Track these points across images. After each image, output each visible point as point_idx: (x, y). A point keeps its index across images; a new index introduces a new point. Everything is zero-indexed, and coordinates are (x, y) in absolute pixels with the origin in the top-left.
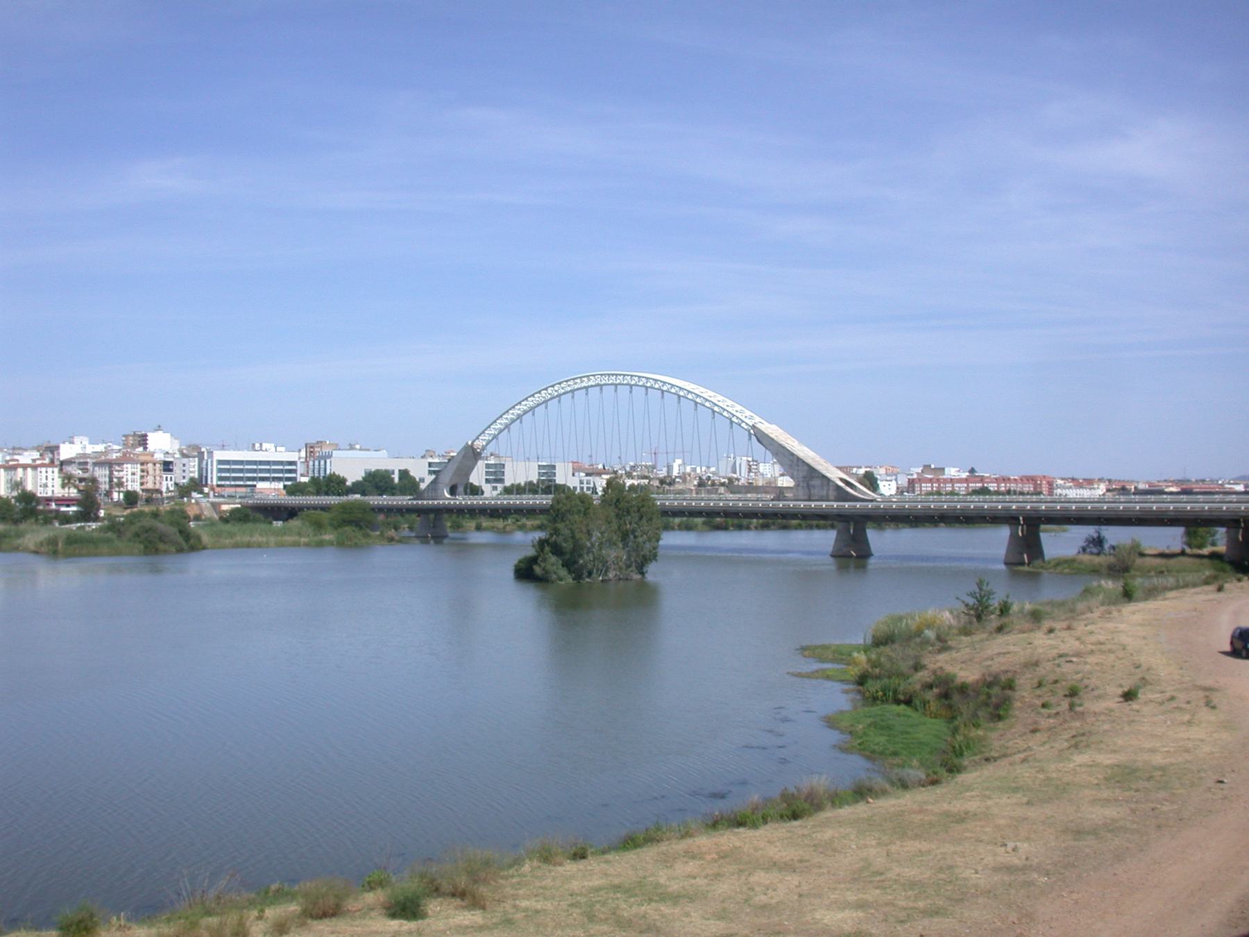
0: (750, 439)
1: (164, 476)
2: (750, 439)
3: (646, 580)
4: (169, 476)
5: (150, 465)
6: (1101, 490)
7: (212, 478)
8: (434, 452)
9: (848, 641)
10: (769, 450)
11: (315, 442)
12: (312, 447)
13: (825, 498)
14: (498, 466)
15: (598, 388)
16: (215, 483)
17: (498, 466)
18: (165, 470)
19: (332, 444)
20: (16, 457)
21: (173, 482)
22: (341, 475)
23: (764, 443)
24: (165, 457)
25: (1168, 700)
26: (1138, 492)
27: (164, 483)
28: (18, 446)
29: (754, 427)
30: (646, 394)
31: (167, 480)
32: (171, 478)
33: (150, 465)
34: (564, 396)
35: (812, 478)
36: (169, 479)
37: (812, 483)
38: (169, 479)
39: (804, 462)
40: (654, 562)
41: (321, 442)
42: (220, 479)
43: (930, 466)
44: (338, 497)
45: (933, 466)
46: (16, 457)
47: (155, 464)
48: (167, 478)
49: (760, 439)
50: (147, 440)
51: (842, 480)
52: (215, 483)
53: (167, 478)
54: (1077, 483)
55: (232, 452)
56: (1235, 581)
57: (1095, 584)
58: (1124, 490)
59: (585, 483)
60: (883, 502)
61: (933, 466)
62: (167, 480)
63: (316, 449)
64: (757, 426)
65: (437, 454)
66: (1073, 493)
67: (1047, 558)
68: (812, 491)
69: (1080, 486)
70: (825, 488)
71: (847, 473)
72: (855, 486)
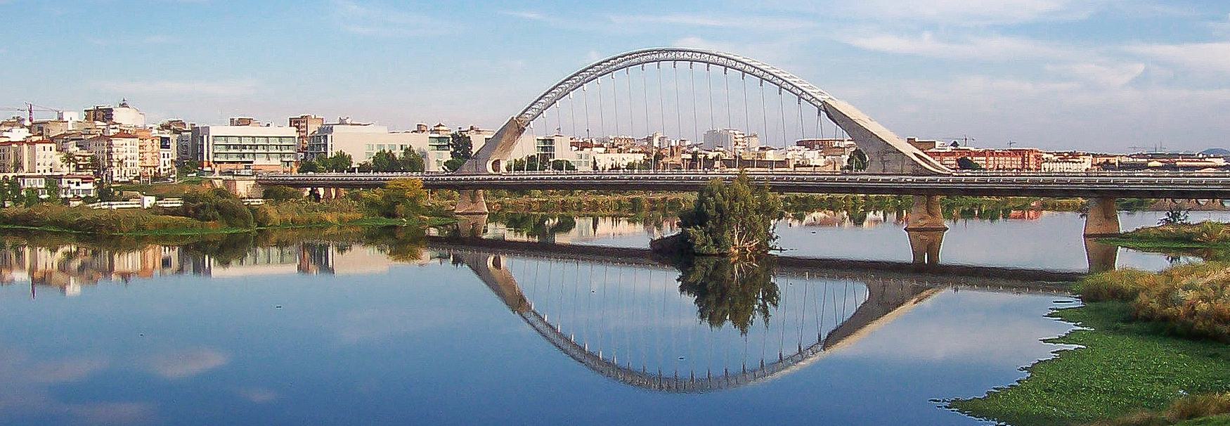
4: (166, 153)
6: (1087, 163)
7: (208, 155)
9: (935, 296)
15: (723, 68)
26: (1123, 166)
27: (162, 160)
29: (824, 103)
31: (164, 157)
35: (886, 153)
36: (166, 156)
38: (166, 156)
45: (917, 140)
48: (164, 154)
54: (1063, 158)
58: (1108, 165)
60: (1015, 176)
61: (917, 140)
62: (164, 157)
66: (1058, 167)
67: (67, 294)
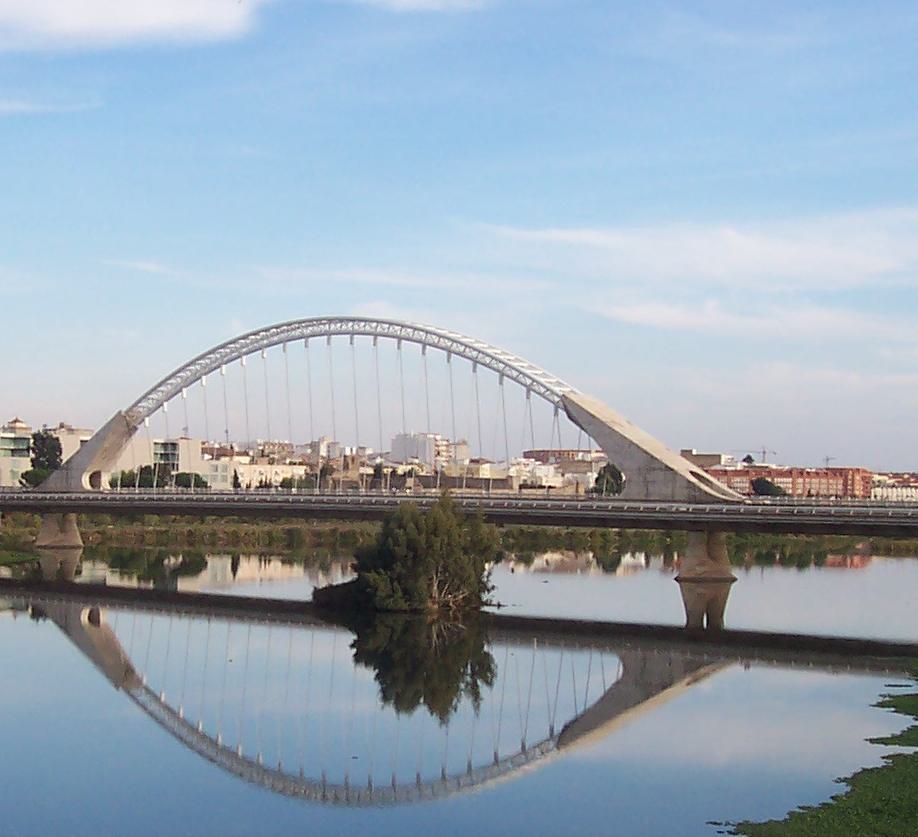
0: (556, 414)
2: (556, 414)
10: (585, 430)
13: (670, 499)
14: (633, 447)
17: (633, 447)
22: (25, 618)
25: (215, 761)
34: (268, 349)
37: (650, 477)
39: (639, 447)
43: (691, 451)
45: (694, 452)
51: (692, 472)
55: (906, 752)
56: (595, 571)
59: (219, 477)
61: (694, 452)
64: (567, 395)
68: (651, 489)
70: (670, 485)
71: (701, 466)
72: (711, 483)
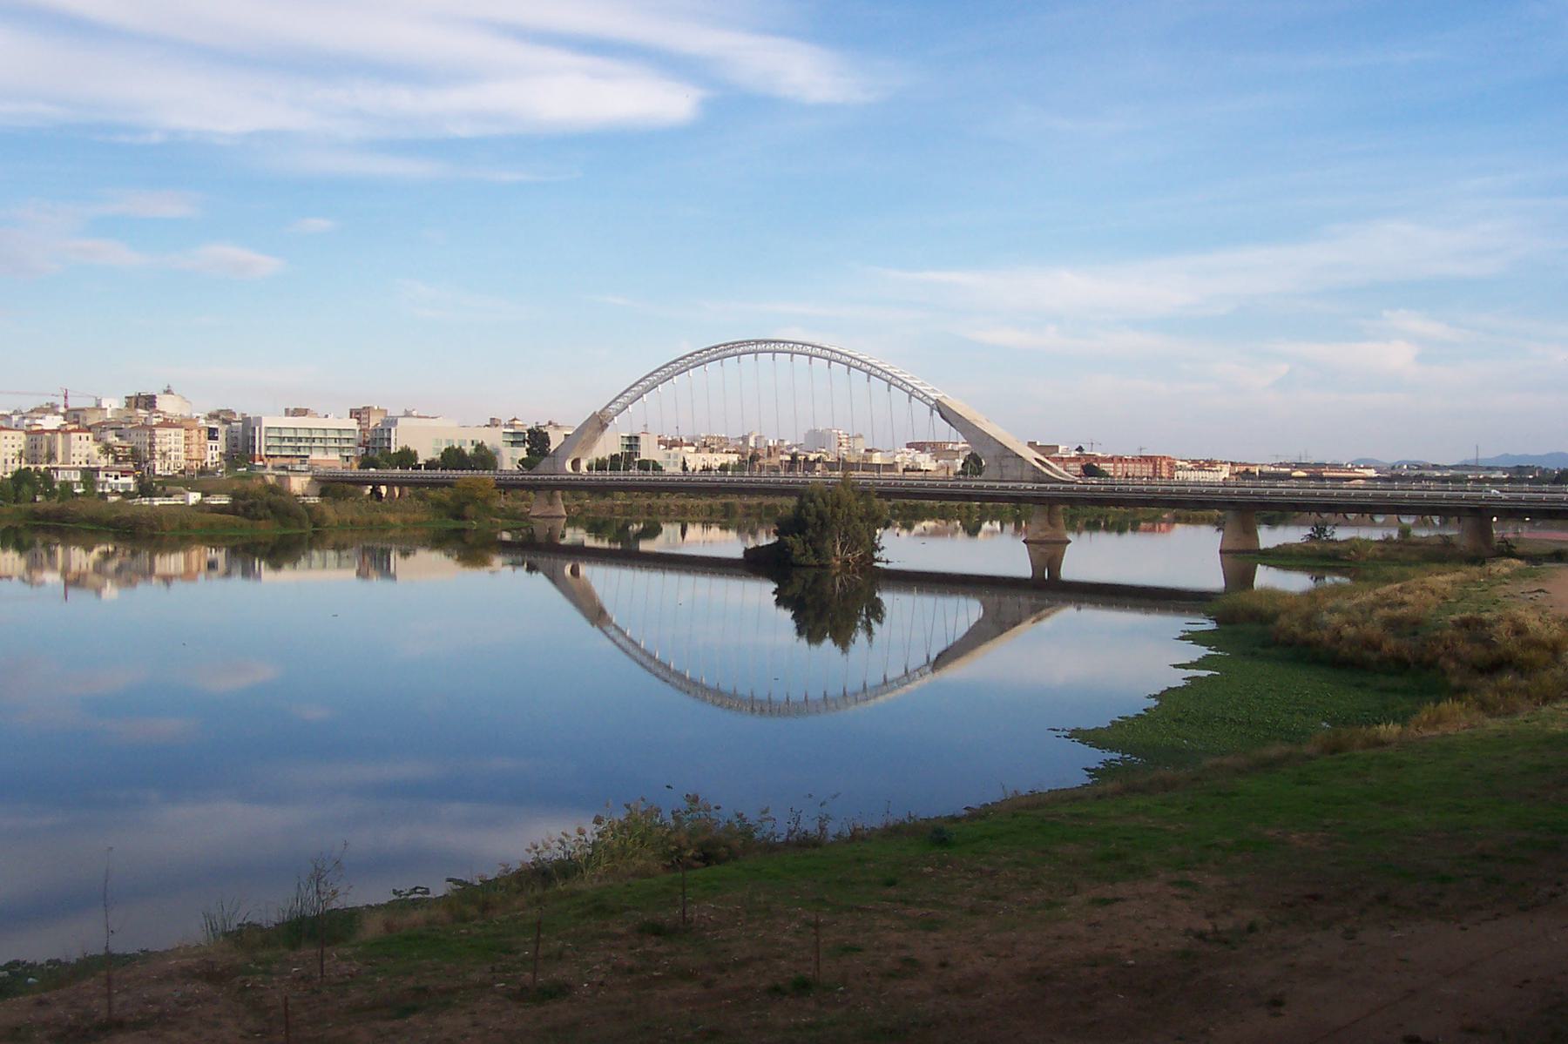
0: (932, 414)
1: (209, 445)
2: (932, 414)
3: (774, 586)
5: (195, 432)
7: (260, 447)
8: (500, 421)
11: (360, 407)
12: (358, 413)
16: (263, 453)
18: (209, 439)
19: (381, 410)
20: (38, 422)
21: (217, 452)
23: (950, 419)
24: (206, 423)
27: (209, 452)
28: (1243, 461)
30: (810, 363)
31: (211, 449)
32: (216, 447)
33: (195, 432)
36: (214, 448)
37: (1004, 463)
38: (214, 448)
39: (995, 440)
40: (1076, 533)
41: (369, 408)
42: (268, 448)
44: (470, 472)
45: (1038, 444)
46: (38, 422)
47: (199, 431)
48: (211, 447)
49: (945, 414)
50: (155, 402)
52: (263, 453)
53: (211, 447)
57: (809, 1019)
59: (672, 463)
61: (1038, 444)
62: (211, 449)
63: (363, 416)
65: (503, 423)
68: (1004, 471)
69: (1201, 468)
72: (1051, 467)
